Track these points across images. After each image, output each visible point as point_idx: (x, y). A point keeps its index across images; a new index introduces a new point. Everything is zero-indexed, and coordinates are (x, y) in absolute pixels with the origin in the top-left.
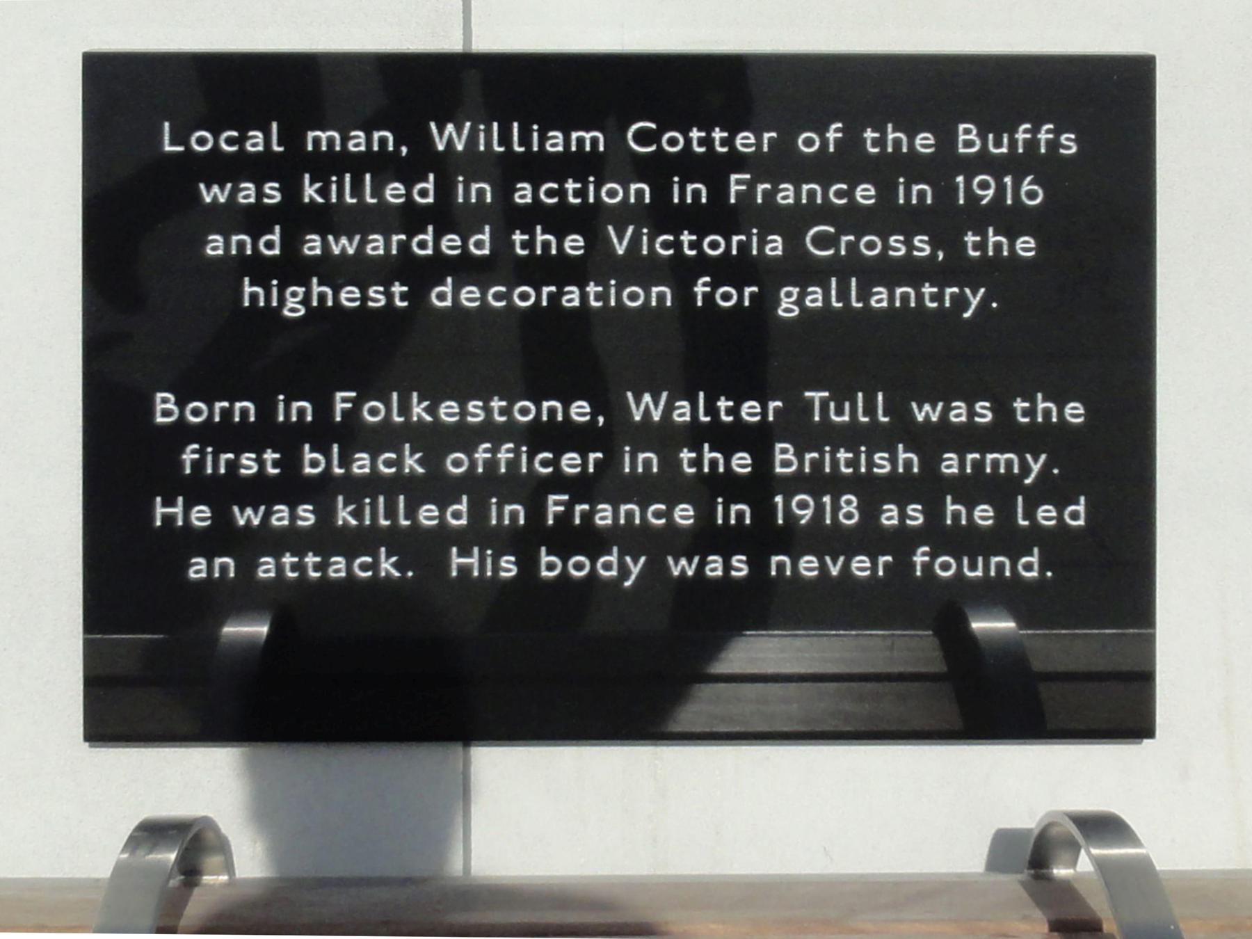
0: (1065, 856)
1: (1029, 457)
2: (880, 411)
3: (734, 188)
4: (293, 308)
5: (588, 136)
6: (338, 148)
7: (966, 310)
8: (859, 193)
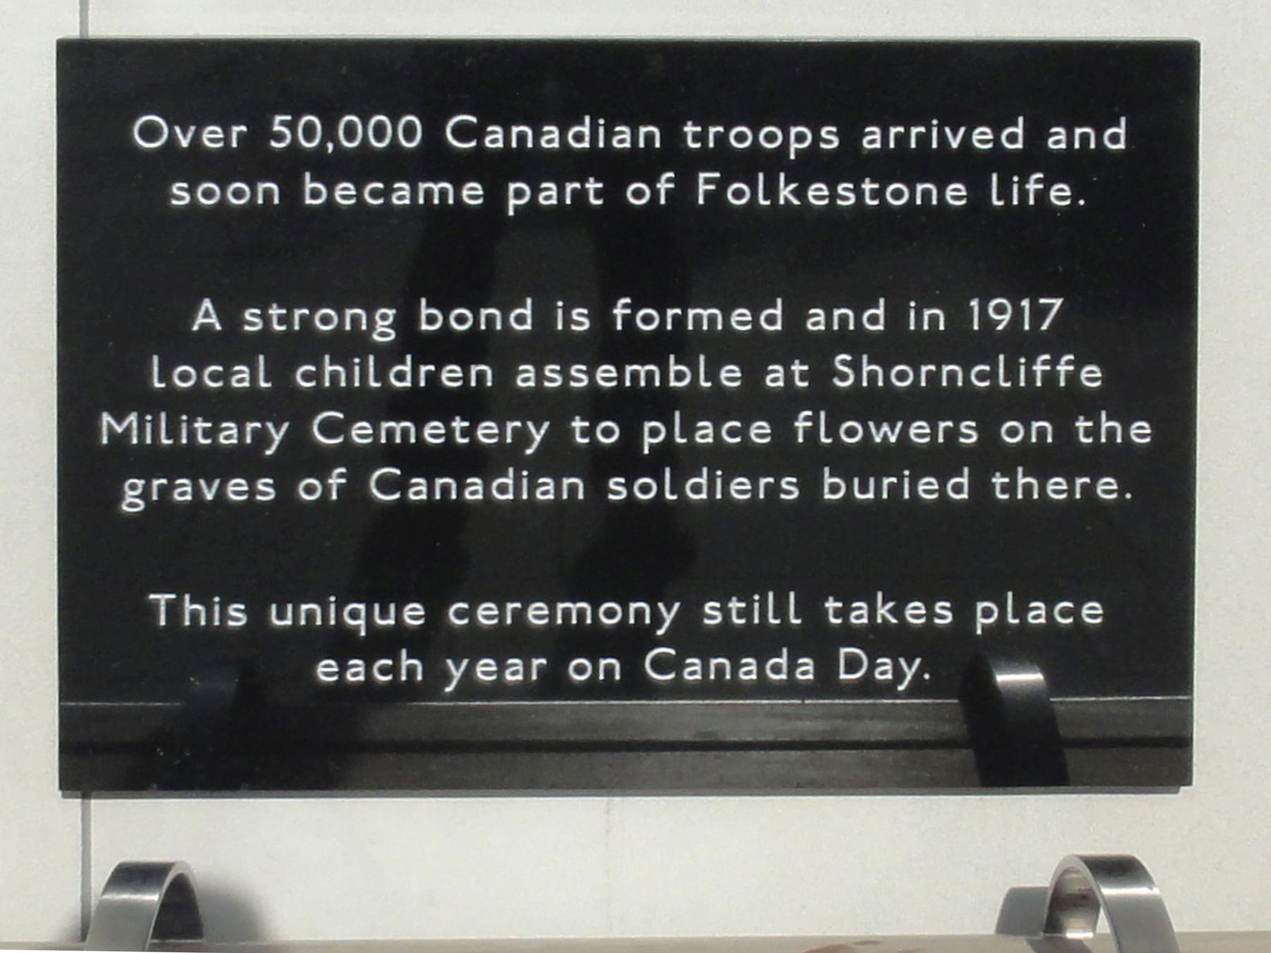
1: (661, 605)
3: (702, 188)
5: (705, 313)
7: (528, 446)
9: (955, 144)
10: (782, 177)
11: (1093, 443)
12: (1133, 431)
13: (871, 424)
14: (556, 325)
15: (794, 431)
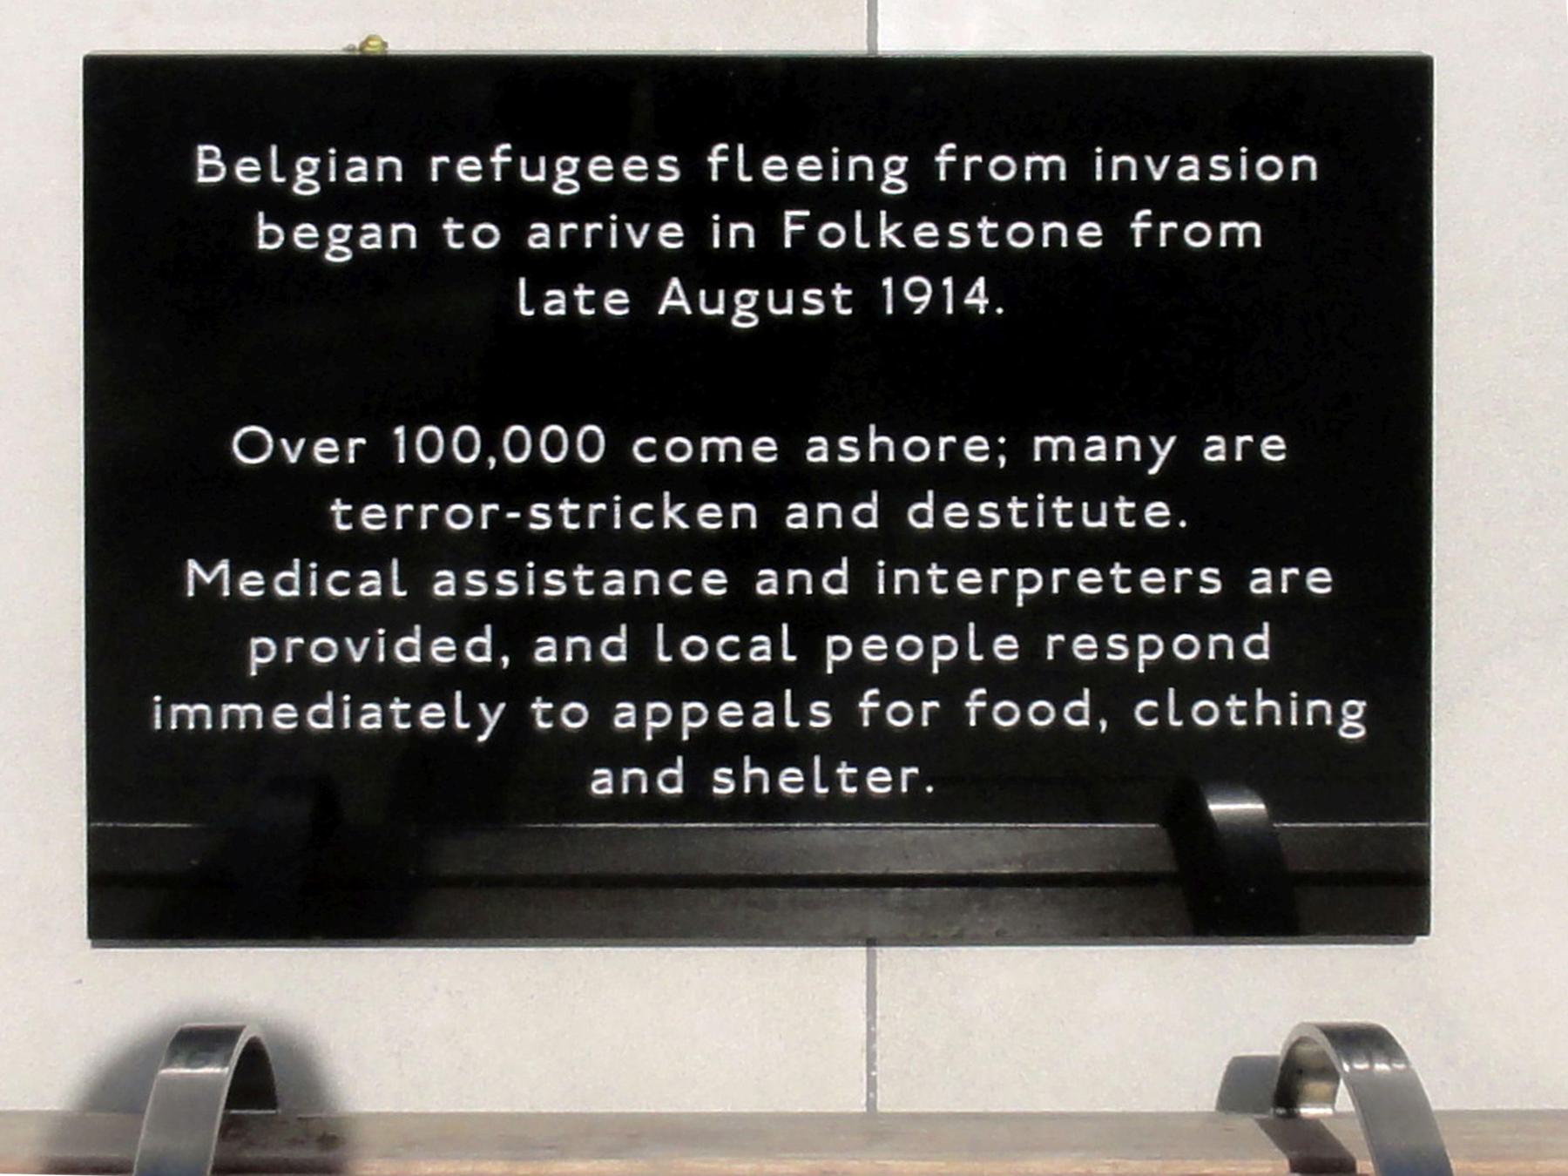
0: (1315, 1087)
3: (789, 228)
9: (638, 243)
11: (1073, 528)
15: (859, 713)
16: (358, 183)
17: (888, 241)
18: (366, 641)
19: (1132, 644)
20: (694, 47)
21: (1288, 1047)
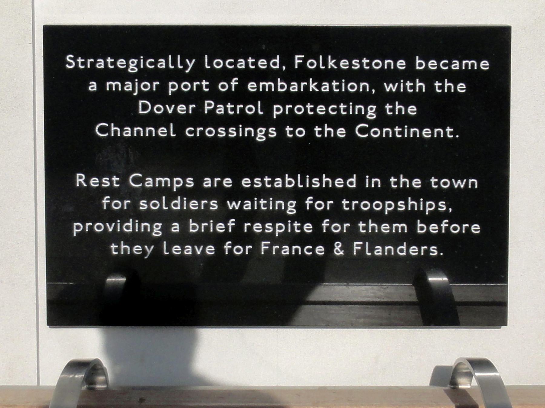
1: (146, 247)
2: (206, 63)
3: (297, 61)
4: (260, 137)
6: (120, 89)
8: (317, 250)
10: (330, 57)
12: (424, 132)
13: (453, 180)
14: (366, 185)
16: (241, 68)
17: (313, 89)
18: (113, 224)
19: (274, 227)
20: (114, 23)
21: (456, 364)
